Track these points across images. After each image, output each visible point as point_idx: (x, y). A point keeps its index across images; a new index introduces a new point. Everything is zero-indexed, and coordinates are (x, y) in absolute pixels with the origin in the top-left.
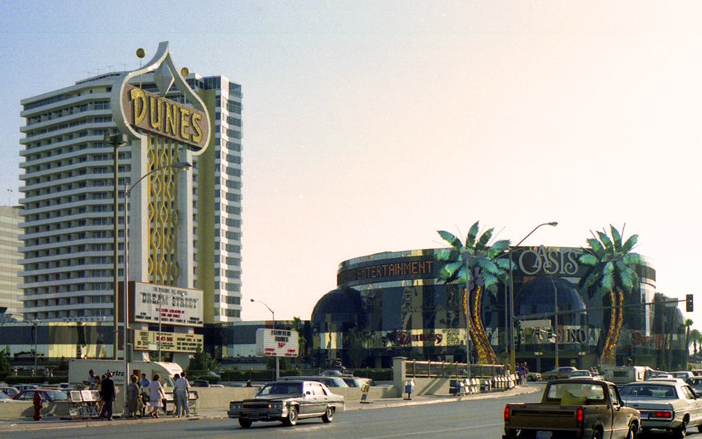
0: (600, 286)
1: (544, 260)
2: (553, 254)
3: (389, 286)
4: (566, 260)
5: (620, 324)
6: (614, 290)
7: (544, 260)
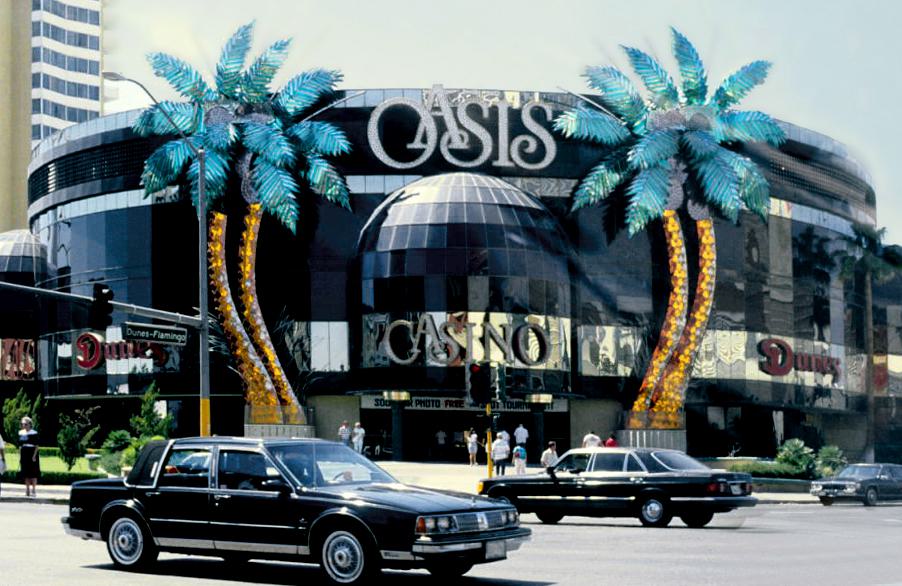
0: (320, 199)
1: (441, 127)
2: (474, 111)
3: (124, 206)
4: (517, 128)
5: (701, 316)
6: (682, 214)
7: (441, 127)
